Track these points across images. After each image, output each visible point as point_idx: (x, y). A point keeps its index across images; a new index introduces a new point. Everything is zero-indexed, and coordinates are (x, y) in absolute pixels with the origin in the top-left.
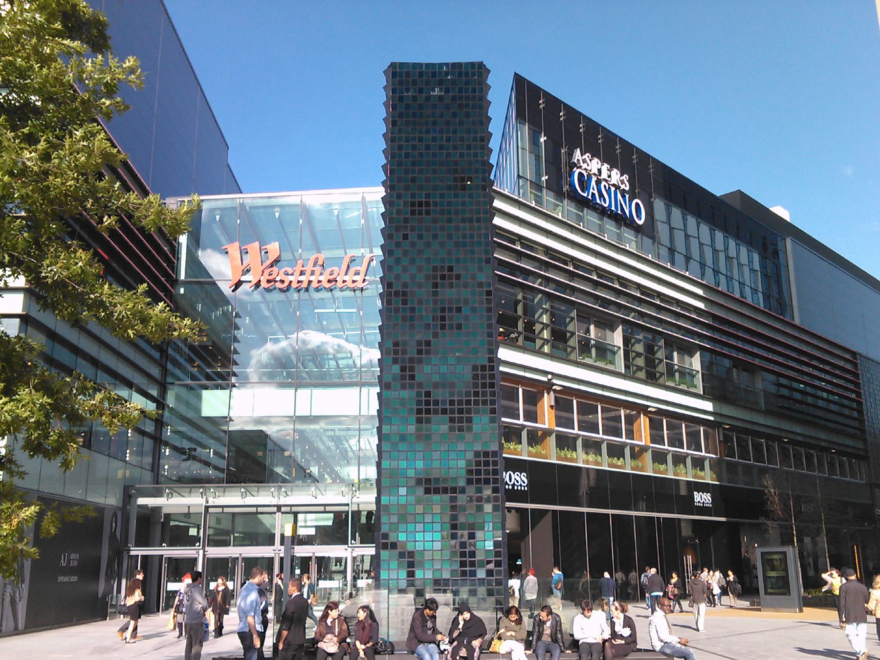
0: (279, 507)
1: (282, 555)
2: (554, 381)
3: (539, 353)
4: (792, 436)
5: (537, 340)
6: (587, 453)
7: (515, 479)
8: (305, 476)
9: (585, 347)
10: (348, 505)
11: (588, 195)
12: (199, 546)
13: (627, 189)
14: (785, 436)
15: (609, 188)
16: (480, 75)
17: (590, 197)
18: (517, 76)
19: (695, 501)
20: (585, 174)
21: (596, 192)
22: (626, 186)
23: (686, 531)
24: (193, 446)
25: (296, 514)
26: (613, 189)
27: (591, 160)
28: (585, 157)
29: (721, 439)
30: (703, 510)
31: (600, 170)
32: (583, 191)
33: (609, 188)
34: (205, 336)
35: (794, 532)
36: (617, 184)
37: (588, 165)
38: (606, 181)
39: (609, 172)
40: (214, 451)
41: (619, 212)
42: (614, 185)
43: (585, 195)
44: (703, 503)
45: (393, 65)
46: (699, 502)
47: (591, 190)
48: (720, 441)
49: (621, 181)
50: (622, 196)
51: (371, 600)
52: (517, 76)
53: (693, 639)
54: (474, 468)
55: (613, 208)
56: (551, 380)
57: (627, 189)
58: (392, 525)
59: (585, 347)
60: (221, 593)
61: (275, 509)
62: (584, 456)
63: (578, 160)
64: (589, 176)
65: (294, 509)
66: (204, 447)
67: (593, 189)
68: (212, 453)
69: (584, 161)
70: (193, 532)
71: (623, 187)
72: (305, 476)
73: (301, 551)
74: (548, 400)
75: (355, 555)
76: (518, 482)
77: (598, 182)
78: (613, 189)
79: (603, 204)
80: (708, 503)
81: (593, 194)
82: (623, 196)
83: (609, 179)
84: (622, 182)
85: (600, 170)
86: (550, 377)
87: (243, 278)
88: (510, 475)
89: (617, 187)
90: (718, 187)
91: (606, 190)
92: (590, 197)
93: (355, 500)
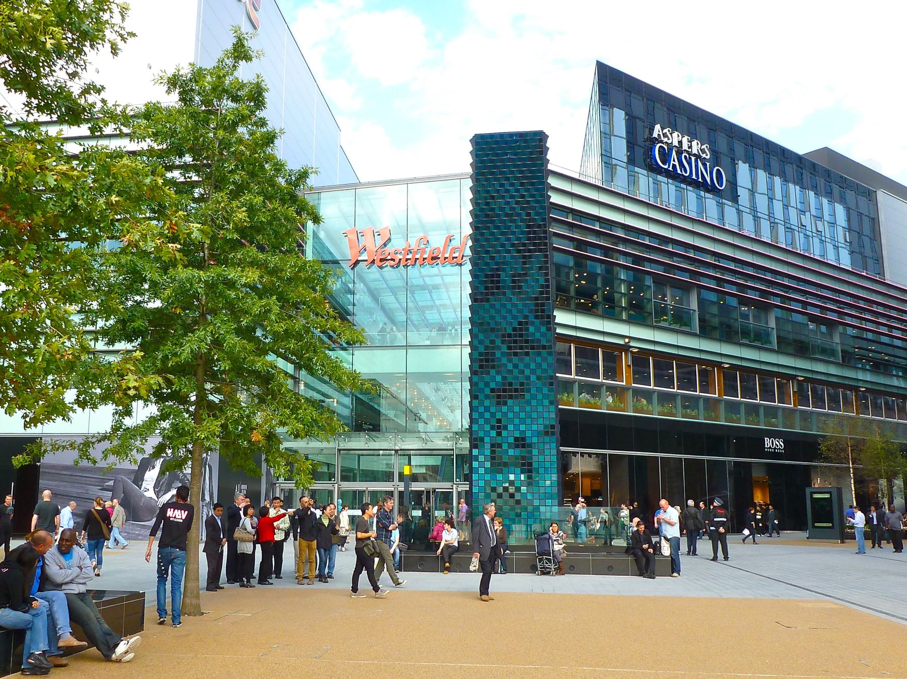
0: (396, 451)
1: (402, 489)
2: (632, 344)
3: (619, 320)
4: (869, 386)
5: (616, 308)
6: (663, 406)
7: (776, 444)
8: (415, 420)
9: (661, 312)
10: (453, 450)
11: (669, 167)
12: (335, 481)
13: (708, 157)
14: (862, 386)
15: (689, 157)
16: (541, 140)
17: (671, 169)
18: (597, 61)
19: (766, 446)
20: (666, 147)
21: (677, 163)
22: (707, 155)
23: (757, 474)
24: (322, 398)
25: (409, 456)
26: (693, 158)
27: (671, 134)
28: (666, 131)
29: (795, 390)
30: (775, 455)
31: (680, 143)
32: (664, 163)
33: (690, 158)
34: (327, 303)
35: (852, 475)
36: (697, 153)
37: (669, 139)
38: (687, 152)
39: (690, 144)
40: (337, 401)
41: (700, 180)
42: (695, 155)
43: (666, 167)
44: (775, 448)
45: (476, 136)
46: (770, 448)
47: (672, 162)
48: (793, 392)
49: (701, 150)
50: (702, 164)
51: (66, 527)
52: (597, 61)
53: (70, 484)
54: (550, 430)
55: (694, 177)
56: (628, 343)
57: (708, 157)
58: (548, 410)
59: (661, 312)
60: (242, 509)
61: (393, 452)
62: (660, 409)
63: (659, 135)
64: (670, 150)
65: (408, 452)
66: (331, 398)
67: (674, 161)
68: (335, 402)
69: (665, 135)
70: (450, 537)
71: (704, 156)
72: (415, 420)
73: (416, 486)
74: (625, 361)
75: (460, 490)
76: (777, 446)
77: (679, 153)
78: (693, 158)
79: (683, 173)
80: (780, 449)
81: (674, 166)
82: (704, 165)
83: (690, 150)
84: (703, 151)
85: (680, 143)
86: (627, 340)
87: (360, 258)
88: (772, 441)
89: (698, 157)
90: (801, 147)
91: (687, 161)
92: (671, 169)
93: (459, 446)
